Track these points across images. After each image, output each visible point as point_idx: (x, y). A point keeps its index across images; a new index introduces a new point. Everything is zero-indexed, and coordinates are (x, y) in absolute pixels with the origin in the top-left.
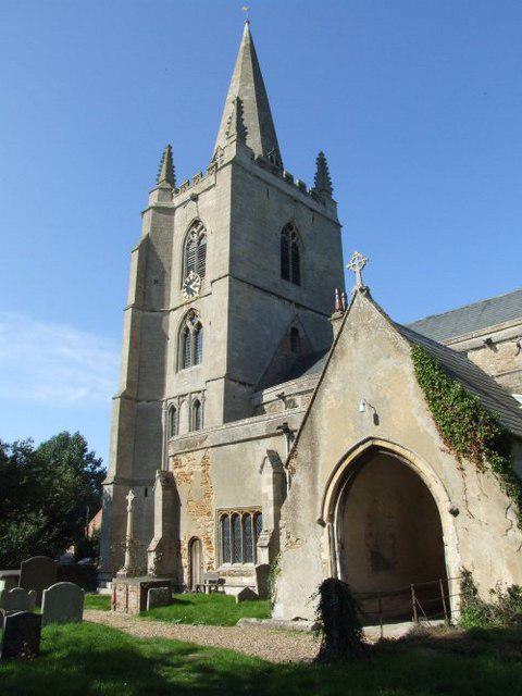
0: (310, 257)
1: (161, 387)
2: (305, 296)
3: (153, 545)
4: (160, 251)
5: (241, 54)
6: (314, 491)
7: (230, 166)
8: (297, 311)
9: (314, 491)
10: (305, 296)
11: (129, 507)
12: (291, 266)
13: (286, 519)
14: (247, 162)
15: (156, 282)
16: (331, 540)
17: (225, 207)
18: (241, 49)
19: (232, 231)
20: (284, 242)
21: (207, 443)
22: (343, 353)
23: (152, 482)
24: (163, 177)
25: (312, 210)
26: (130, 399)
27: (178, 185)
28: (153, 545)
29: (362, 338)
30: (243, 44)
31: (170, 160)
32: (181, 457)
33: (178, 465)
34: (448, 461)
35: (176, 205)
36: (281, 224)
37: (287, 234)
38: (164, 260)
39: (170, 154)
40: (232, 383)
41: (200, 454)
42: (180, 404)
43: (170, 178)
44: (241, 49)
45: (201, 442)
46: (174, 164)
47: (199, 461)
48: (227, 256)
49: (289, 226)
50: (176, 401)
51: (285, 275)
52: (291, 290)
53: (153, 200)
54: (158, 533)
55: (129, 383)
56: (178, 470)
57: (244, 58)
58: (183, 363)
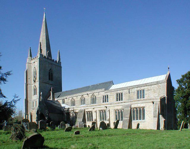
0: (55, 75)
12: (51, 77)
20: (49, 73)
36: (49, 69)
49: (51, 69)
51: (49, 79)
52: (51, 82)
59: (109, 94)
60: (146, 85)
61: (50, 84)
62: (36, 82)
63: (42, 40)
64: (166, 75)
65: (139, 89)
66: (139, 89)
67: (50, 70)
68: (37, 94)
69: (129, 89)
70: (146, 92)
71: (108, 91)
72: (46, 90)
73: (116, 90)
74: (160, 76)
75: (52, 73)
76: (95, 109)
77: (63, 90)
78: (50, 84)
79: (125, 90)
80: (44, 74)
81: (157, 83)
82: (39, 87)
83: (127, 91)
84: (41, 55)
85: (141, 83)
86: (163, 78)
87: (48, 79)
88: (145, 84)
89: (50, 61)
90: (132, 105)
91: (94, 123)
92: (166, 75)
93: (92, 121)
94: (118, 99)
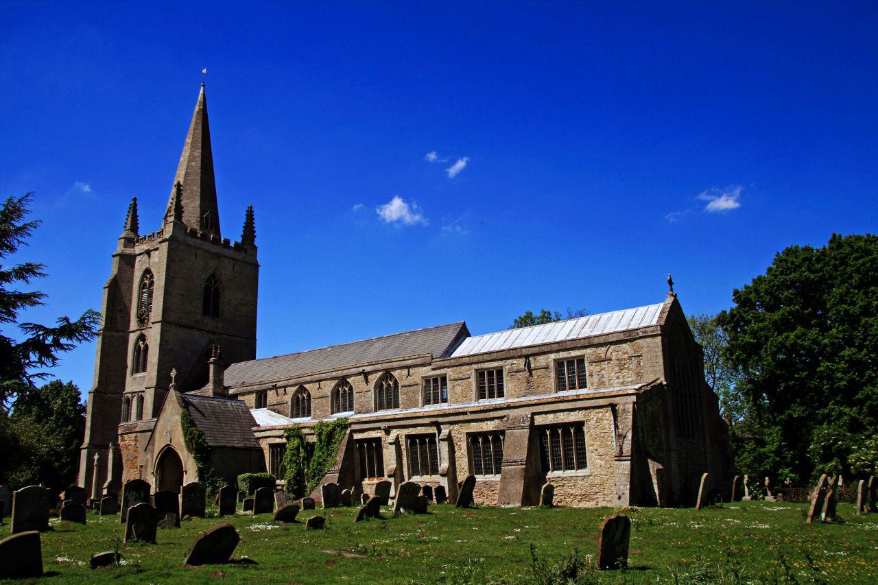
0: (230, 298)
1: (123, 385)
2: (220, 325)
3: (106, 485)
4: (124, 288)
5: (194, 120)
6: (152, 461)
7: (167, 243)
8: (212, 336)
9: (152, 461)
10: (220, 325)
11: (95, 463)
12: (211, 299)
13: (602, 520)
14: (181, 236)
15: (121, 311)
16: (156, 481)
17: (162, 272)
18: (195, 114)
19: (165, 289)
20: (207, 288)
21: (137, 429)
22: (165, 410)
23: (108, 448)
24: (128, 227)
25: (233, 259)
26: (100, 392)
27: (141, 233)
28: (106, 485)
29: (171, 406)
30: (197, 109)
31: (135, 211)
32: (125, 436)
33: (123, 440)
34: (186, 452)
35: (137, 252)
36: (204, 276)
37: (211, 282)
38: (126, 301)
39: (135, 205)
40: (160, 390)
41: (134, 435)
42: (133, 397)
43: (134, 228)
44: (195, 114)
45: (135, 428)
46: (138, 214)
47: (133, 439)
48: (161, 307)
49: (213, 276)
50: (130, 395)
51: (206, 312)
52: (210, 323)
53: (120, 248)
54: (109, 478)
55: (100, 382)
56: (122, 443)
57: (196, 124)
58: (136, 370)
59: (449, 372)
60: (589, 343)
61: (208, 331)
62: (150, 325)
63: (187, 174)
64: (662, 305)
65: (563, 355)
66: (563, 355)
67: (209, 280)
68: (149, 367)
69: (528, 354)
70: (591, 368)
71: (447, 363)
72: (189, 354)
73: (476, 359)
74: (641, 310)
75: (217, 290)
76: (394, 433)
77: (258, 357)
78: (208, 331)
79: (510, 361)
80: (182, 295)
81: (630, 337)
82: (161, 345)
83: (520, 363)
84: (179, 224)
85: (550, 340)
86: (650, 315)
87: (200, 311)
88: (584, 338)
89: (215, 249)
90: (536, 417)
91: (383, 489)
92: (662, 305)
93: (381, 474)
94: (496, 391)
